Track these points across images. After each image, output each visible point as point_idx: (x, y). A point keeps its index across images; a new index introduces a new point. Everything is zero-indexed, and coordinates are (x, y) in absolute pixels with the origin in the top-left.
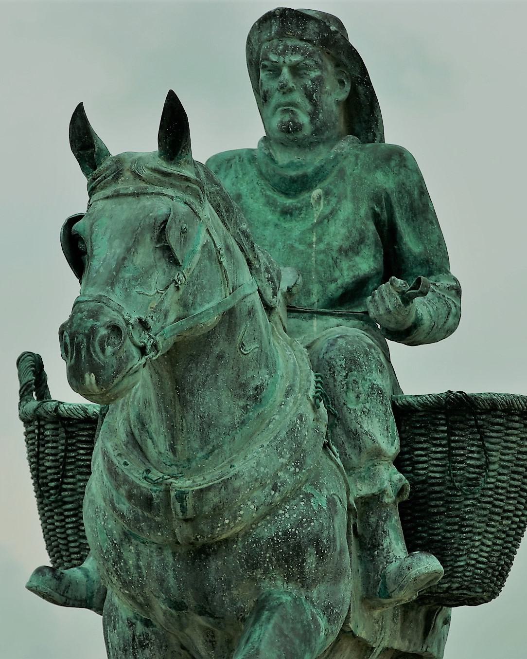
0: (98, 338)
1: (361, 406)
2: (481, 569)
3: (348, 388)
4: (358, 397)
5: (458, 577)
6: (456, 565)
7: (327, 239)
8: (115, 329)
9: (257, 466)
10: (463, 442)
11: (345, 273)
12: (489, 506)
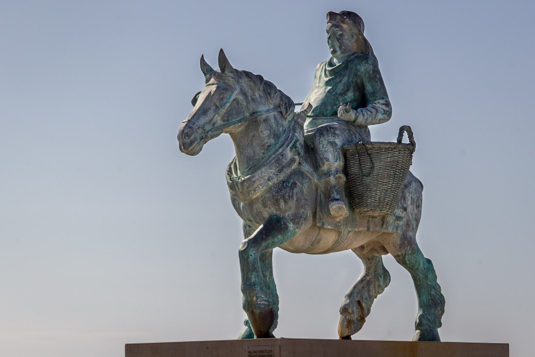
2: (377, 203)
3: (320, 143)
5: (369, 206)
6: (367, 202)
9: (261, 173)
10: (364, 160)
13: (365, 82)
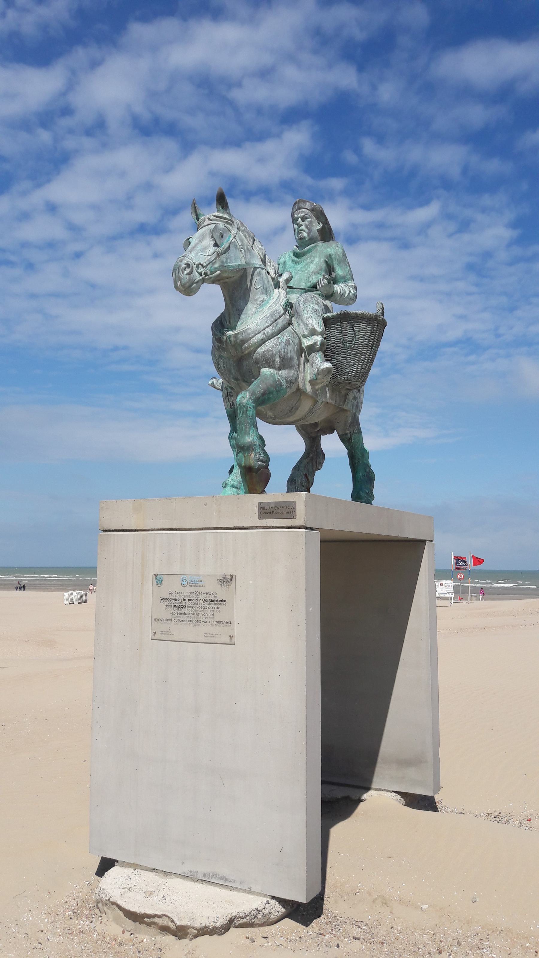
0: (181, 268)
1: (308, 315)
3: (304, 309)
4: (308, 312)
7: (309, 269)
8: (188, 265)
9: (256, 326)
11: (314, 279)
12: (356, 351)
13: (335, 264)
